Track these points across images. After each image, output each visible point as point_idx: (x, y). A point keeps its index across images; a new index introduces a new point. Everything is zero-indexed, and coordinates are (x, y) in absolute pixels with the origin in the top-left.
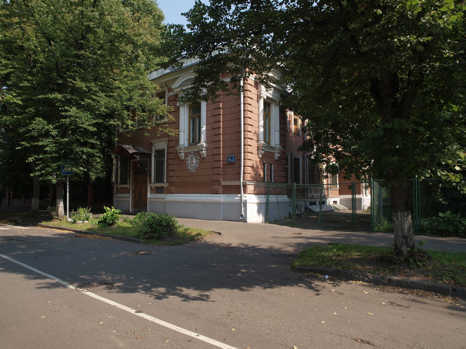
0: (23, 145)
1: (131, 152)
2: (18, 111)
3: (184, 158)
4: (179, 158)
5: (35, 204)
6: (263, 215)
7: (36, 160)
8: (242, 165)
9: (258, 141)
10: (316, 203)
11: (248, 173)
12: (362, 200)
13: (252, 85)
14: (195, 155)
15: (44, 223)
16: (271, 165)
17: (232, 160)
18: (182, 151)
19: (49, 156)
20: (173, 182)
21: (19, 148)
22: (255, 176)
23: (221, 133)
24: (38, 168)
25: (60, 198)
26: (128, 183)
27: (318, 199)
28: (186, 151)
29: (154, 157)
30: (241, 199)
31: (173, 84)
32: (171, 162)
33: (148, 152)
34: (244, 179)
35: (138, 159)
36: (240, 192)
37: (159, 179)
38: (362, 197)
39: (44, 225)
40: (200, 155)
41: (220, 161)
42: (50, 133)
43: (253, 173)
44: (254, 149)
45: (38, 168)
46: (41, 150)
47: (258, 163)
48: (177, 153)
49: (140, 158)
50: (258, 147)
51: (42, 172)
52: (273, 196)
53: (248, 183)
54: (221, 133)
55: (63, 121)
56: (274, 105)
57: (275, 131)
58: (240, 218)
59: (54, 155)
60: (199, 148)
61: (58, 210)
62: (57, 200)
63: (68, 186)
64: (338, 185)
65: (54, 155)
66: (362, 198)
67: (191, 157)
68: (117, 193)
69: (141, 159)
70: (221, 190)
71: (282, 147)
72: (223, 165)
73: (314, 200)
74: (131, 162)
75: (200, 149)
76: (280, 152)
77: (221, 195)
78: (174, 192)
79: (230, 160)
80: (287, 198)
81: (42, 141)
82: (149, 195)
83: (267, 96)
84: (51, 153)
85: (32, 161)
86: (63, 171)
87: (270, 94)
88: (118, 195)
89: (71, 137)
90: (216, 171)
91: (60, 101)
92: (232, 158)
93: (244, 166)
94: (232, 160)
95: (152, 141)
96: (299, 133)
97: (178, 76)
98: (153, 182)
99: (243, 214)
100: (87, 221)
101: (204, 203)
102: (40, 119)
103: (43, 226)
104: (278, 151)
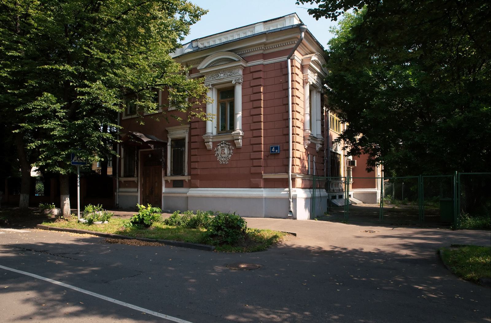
0: (23, 127)
1: (145, 141)
2: (4, 86)
3: (212, 147)
5: (24, 200)
6: (308, 210)
7: (42, 146)
8: (291, 156)
9: (304, 130)
10: (336, 197)
11: (297, 165)
12: (377, 194)
13: (299, 69)
14: (227, 145)
15: (45, 224)
17: (277, 151)
18: (211, 140)
19: (58, 142)
20: (198, 175)
21: (17, 131)
22: (302, 168)
23: (262, 120)
24: (42, 156)
25: (66, 194)
26: (135, 176)
27: (337, 193)
28: (215, 140)
29: (170, 147)
30: (290, 194)
31: (200, 63)
34: (292, 172)
35: (153, 148)
36: (288, 186)
37: (178, 169)
38: (377, 191)
39: (48, 227)
40: (234, 145)
41: (262, 151)
42: (56, 114)
43: (300, 166)
44: (300, 139)
45: (42, 156)
46: (45, 134)
47: (304, 154)
48: (203, 142)
49: (154, 147)
50: (304, 137)
51: (48, 161)
53: (297, 176)
54: (262, 120)
55: (81, 98)
57: (316, 120)
58: (289, 215)
59: (63, 140)
60: (233, 136)
61: (63, 208)
62: (61, 196)
63: (78, 179)
64: (352, 179)
65: (63, 140)
66: (378, 192)
68: (119, 187)
69: (156, 149)
70: (262, 184)
72: (264, 156)
73: (334, 194)
75: (235, 138)
77: (262, 189)
78: (199, 187)
80: (326, 193)
81: (46, 123)
82: (164, 190)
83: (313, 82)
84: (60, 137)
85: (34, 147)
86: (73, 161)
87: (315, 80)
88: (121, 190)
89: (86, 119)
90: (256, 163)
91: (71, 74)
92: (276, 148)
93: (293, 157)
95: (167, 129)
97: (205, 55)
98: (170, 175)
99: (292, 211)
101: (241, 199)
102: (49, 94)
103: (45, 228)
104: (320, 142)
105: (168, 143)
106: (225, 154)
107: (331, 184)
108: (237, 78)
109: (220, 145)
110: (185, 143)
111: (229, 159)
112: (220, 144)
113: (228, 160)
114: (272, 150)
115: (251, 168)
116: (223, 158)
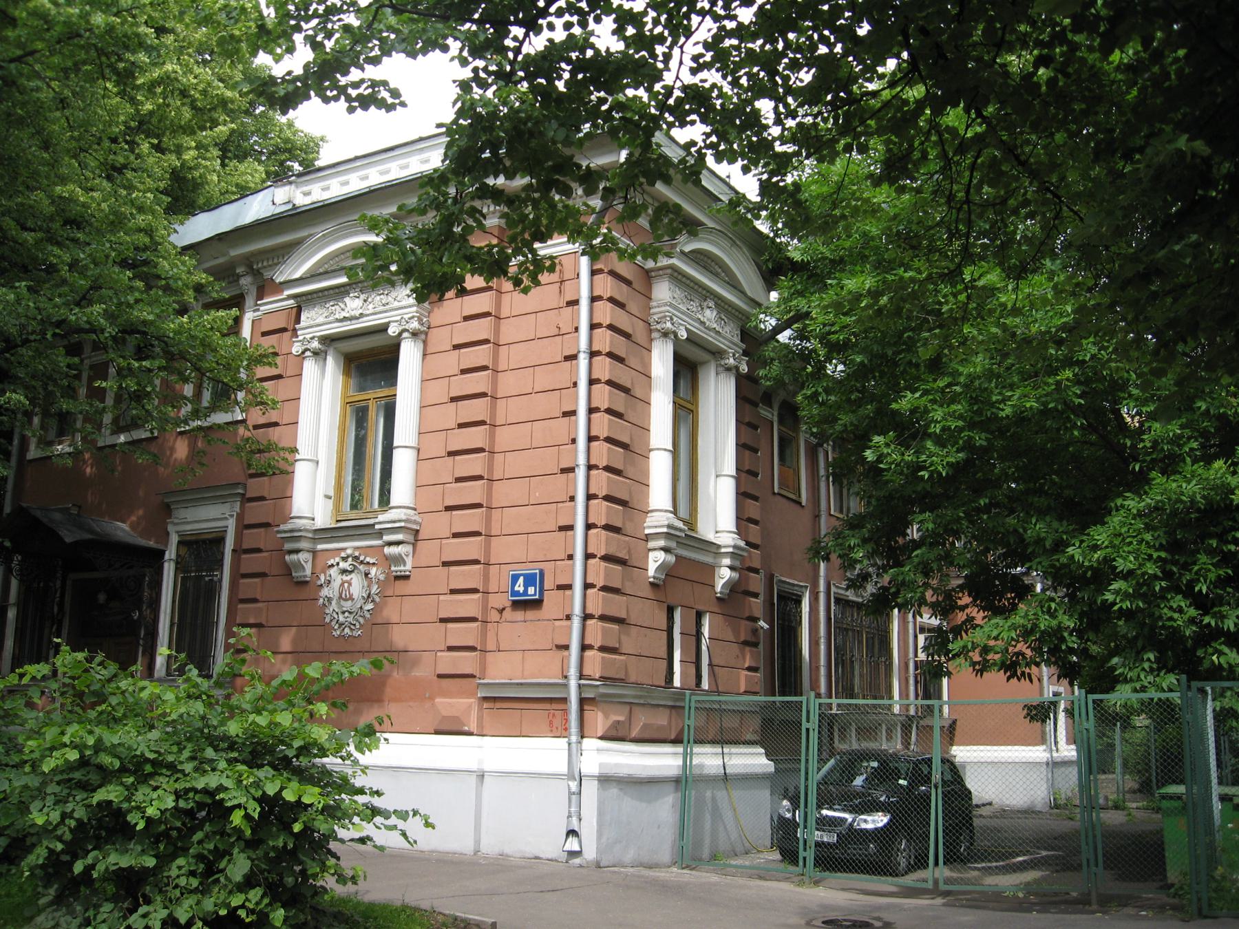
1: (68, 540)
4: (288, 570)
16: (699, 615)
17: (531, 590)
18: (304, 545)
29: (173, 565)
32: (249, 587)
33: (151, 544)
52: (708, 749)
56: (713, 373)
67: (344, 571)
71: (748, 543)
74: (69, 583)
76: (737, 564)
78: (473, 727)
79: (521, 589)
80: (766, 761)
92: (529, 581)
94: (531, 590)
96: (800, 496)
98: (163, 673)
100: (238, 878)
105: (167, 553)
106: (351, 598)
107: (836, 729)
108: (405, 316)
109: (338, 564)
110: (223, 554)
111: (364, 617)
112: (337, 559)
113: (361, 620)
114: (516, 588)
115: (439, 654)
116: (343, 613)
